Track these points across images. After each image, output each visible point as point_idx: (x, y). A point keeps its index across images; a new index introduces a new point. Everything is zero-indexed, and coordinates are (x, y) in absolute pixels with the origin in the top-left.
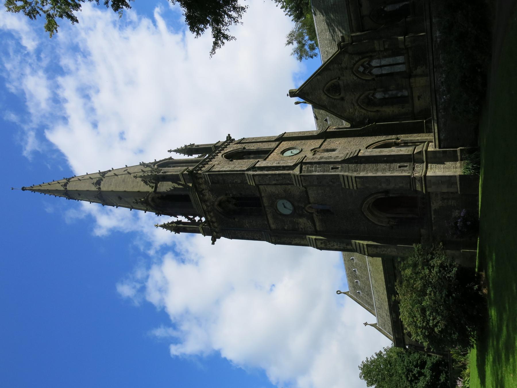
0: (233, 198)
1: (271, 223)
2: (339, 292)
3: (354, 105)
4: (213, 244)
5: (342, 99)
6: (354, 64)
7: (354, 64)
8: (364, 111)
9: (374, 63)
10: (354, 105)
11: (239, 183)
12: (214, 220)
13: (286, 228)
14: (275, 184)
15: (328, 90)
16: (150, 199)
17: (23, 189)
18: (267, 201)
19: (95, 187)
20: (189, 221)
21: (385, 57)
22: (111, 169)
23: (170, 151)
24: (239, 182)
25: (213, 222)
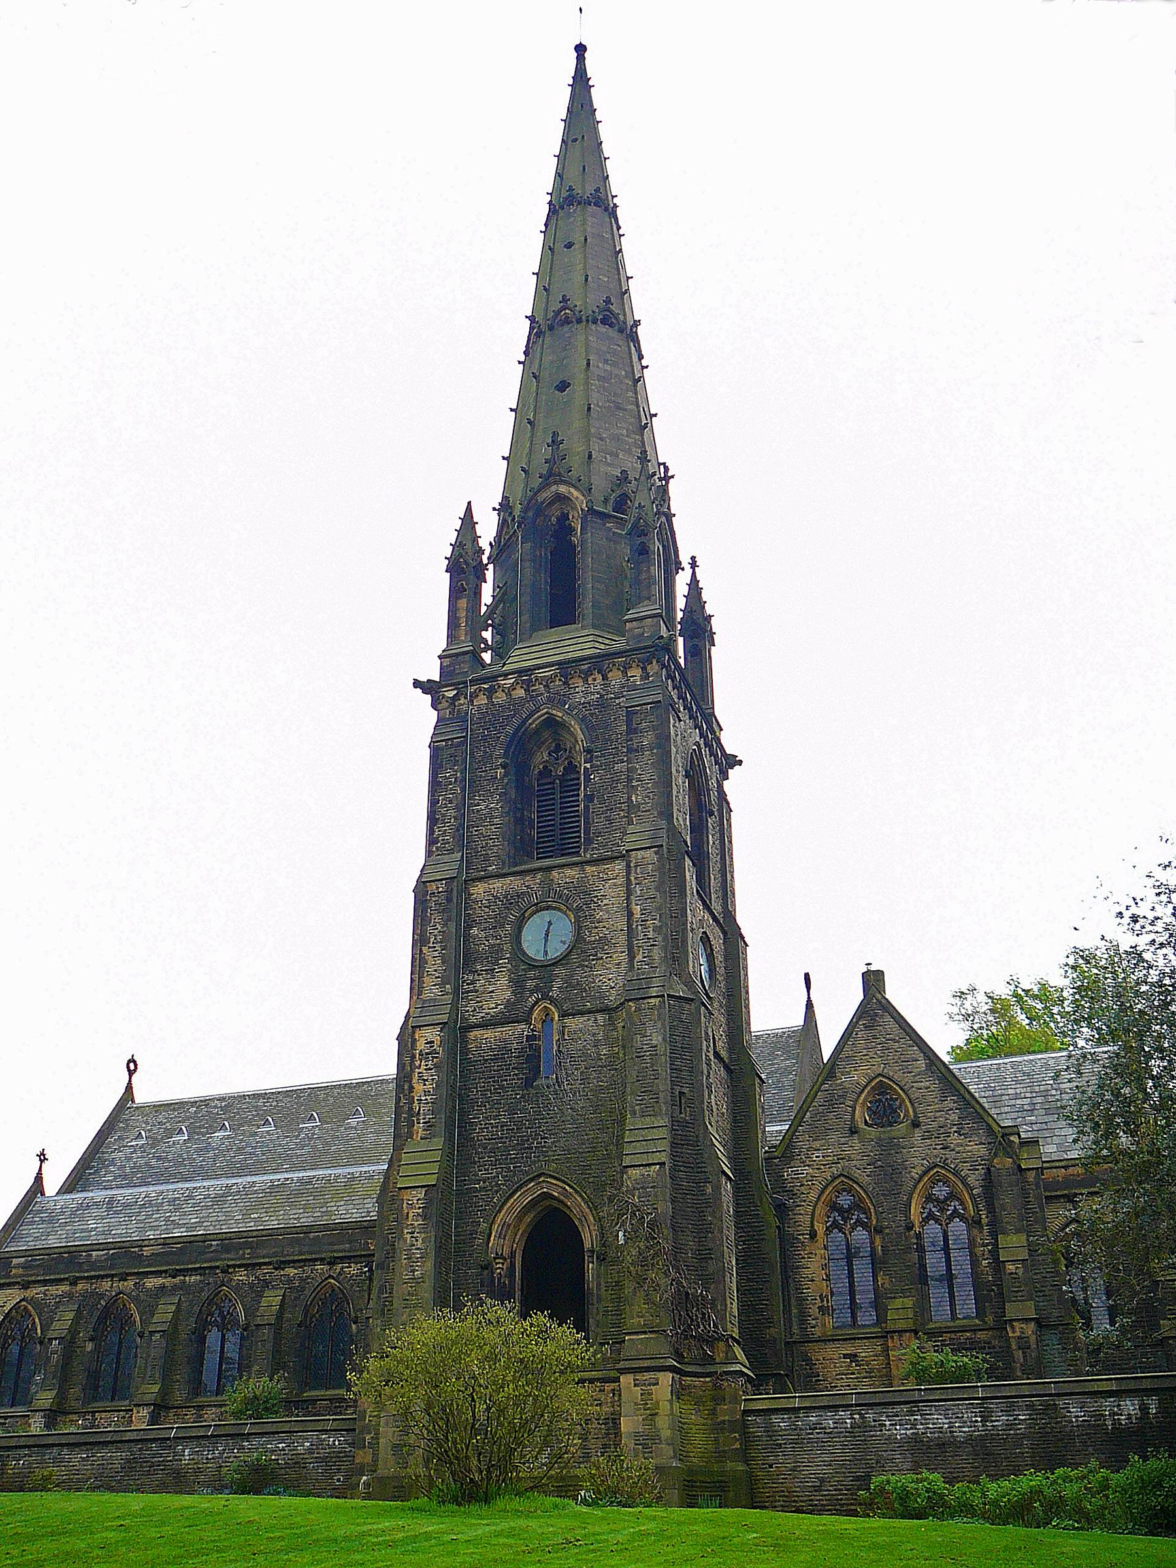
0: (572, 768)
2: (132, 1066)
4: (414, 683)
5: (853, 1131)
6: (956, 1173)
7: (956, 1173)
8: (813, 1195)
9: (958, 1228)
11: (629, 798)
12: (500, 697)
13: (474, 931)
14: (630, 914)
15: (882, 1089)
16: (563, 489)
17: (581, 49)
20: (484, 609)
22: (644, 364)
23: (694, 564)
25: (491, 692)
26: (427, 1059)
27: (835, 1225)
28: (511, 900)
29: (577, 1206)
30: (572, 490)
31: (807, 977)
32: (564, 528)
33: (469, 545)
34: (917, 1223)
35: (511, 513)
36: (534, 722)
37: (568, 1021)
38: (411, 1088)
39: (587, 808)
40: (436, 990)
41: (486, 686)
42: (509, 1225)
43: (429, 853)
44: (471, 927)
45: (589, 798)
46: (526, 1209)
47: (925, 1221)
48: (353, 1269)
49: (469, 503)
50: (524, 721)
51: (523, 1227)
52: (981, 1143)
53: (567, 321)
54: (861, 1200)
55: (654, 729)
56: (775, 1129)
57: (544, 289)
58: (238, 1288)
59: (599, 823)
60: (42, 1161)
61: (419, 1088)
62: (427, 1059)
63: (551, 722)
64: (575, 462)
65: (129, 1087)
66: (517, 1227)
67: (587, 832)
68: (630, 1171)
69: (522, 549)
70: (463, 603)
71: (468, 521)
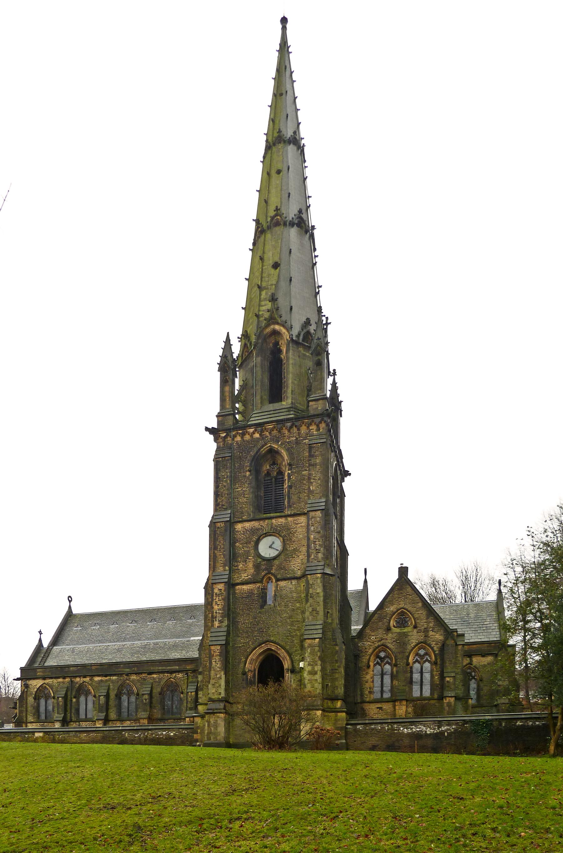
1: (244, 525)
2: (70, 599)
3: (379, 641)
8: (371, 651)
9: (427, 665)
10: (379, 641)
11: (309, 487)
12: (247, 437)
13: (237, 544)
14: (309, 539)
16: (277, 327)
17: (284, 21)
18: (280, 523)
19: (295, 215)
20: (236, 392)
21: (432, 676)
24: (311, 488)
25: (243, 435)
26: (219, 596)
27: (378, 663)
28: (253, 531)
29: (282, 654)
30: (282, 328)
31: (365, 570)
32: (276, 351)
33: (229, 358)
34: (411, 663)
35: (249, 340)
36: (264, 450)
37: (279, 583)
38: (213, 608)
39: (289, 491)
40: (221, 569)
41: (241, 432)
42: (254, 660)
43: (216, 510)
44: (236, 543)
45: (290, 487)
46: (260, 654)
47: (414, 663)
48: (180, 675)
49: (228, 333)
50: (260, 449)
51: (259, 660)
52: (441, 635)
53: (277, 224)
54: (389, 654)
55: (322, 455)
56: (356, 627)
57: (264, 202)
58: (133, 681)
59: (294, 498)
60: (40, 634)
61: (216, 607)
62: (219, 596)
63: (272, 451)
64: (284, 311)
65: (70, 607)
66: (256, 661)
67: (289, 502)
68: (307, 640)
69: (256, 360)
70: (227, 389)
71: (228, 342)
